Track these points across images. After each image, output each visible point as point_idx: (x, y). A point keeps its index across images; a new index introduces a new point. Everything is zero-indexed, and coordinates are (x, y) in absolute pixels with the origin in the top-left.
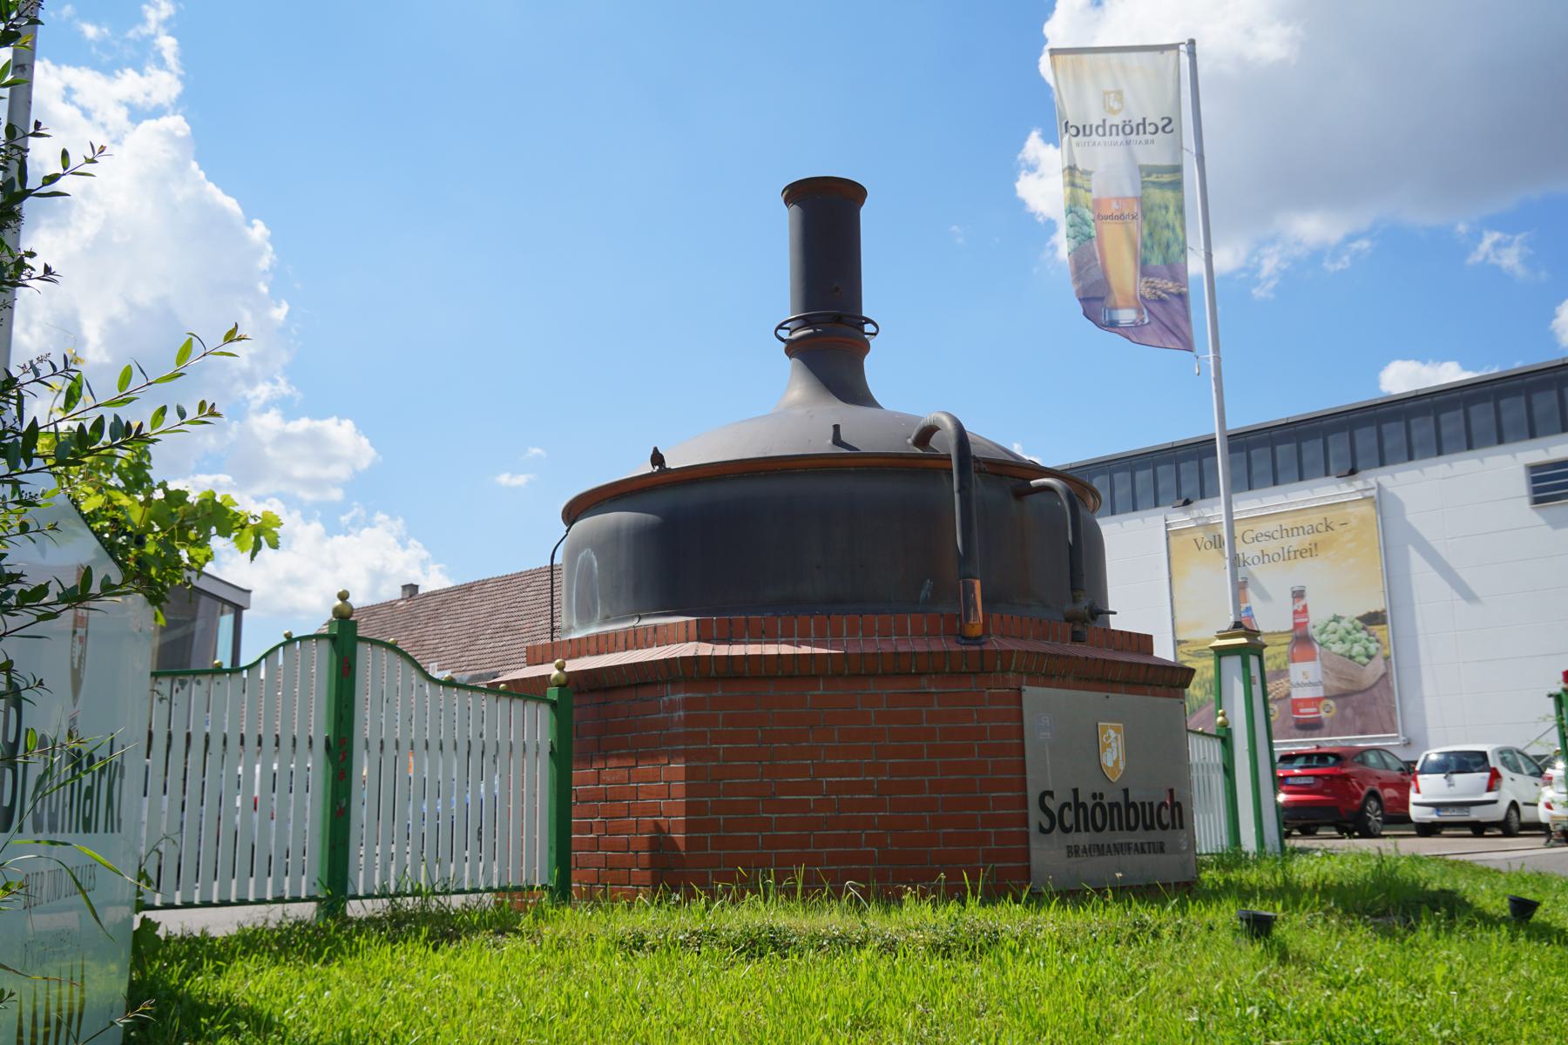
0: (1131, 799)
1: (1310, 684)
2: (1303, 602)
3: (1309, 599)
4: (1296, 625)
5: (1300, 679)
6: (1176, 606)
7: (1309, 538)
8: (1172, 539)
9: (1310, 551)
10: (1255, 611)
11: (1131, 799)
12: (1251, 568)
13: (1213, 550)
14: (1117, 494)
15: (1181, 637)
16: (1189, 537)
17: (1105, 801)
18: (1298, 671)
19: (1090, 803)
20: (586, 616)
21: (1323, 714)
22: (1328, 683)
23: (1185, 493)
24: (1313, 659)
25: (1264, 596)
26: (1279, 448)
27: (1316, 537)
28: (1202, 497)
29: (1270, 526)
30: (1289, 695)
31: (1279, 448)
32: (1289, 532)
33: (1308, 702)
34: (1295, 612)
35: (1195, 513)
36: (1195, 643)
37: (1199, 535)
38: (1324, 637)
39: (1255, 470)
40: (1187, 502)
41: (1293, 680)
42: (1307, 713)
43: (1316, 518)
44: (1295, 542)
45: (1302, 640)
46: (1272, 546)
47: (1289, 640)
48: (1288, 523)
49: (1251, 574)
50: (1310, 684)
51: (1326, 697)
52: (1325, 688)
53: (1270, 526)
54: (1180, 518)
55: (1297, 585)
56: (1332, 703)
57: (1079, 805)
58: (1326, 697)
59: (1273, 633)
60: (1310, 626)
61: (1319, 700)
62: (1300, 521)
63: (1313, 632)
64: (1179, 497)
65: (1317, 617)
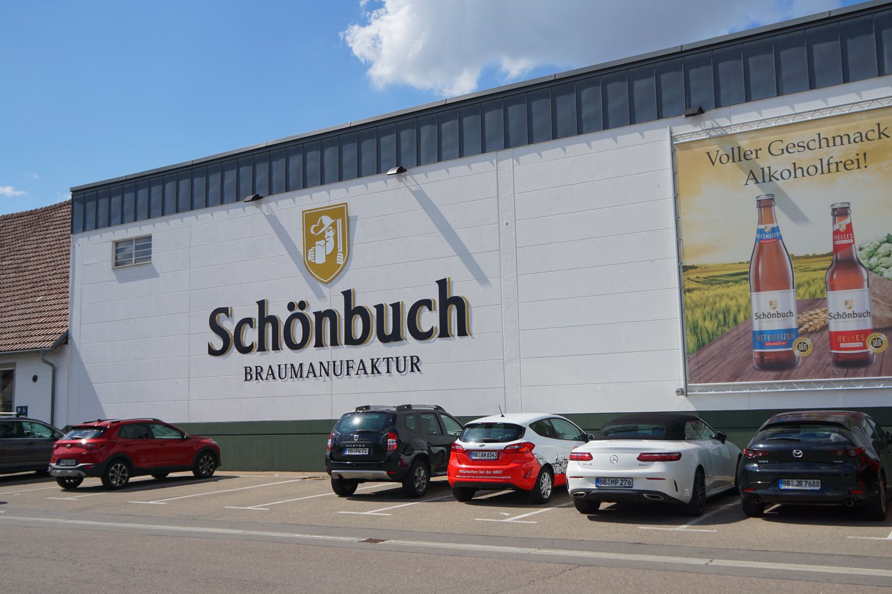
0: (358, 302)
1: (854, 315)
2: (848, 221)
3: (855, 218)
4: (837, 248)
5: (842, 309)
6: (683, 227)
7: (855, 148)
8: (679, 153)
9: (859, 162)
10: (783, 232)
11: (358, 302)
12: (780, 183)
13: (730, 164)
14: (611, 106)
15: (688, 262)
16: (701, 150)
17: (310, 313)
18: (838, 300)
19: (283, 315)
20: (428, 421)
21: (871, 349)
22: (878, 313)
23: (695, 102)
24: (859, 286)
25: (797, 216)
26: (816, 48)
27: (866, 146)
28: (718, 105)
29: (807, 135)
30: (826, 327)
31: (816, 48)
32: (830, 142)
33: (850, 335)
34: (836, 233)
35: (708, 124)
36: (706, 268)
37: (713, 148)
38: (874, 261)
39: (784, 73)
40: (701, 111)
41: (832, 309)
42: (849, 348)
43: (865, 125)
44: (837, 153)
45: (844, 265)
46: (805, 159)
47: (828, 264)
48: (827, 131)
49: (779, 190)
50: (854, 315)
51: (874, 330)
52: (874, 318)
53: (807, 135)
54: (686, 129)
55: (839, 202)
56: (883, 337)
57: (266, 319)
58: (874, 330)
59: (807, 257)
60: (857, 244)
61: (866, 333)
62: (843, 127)
63: (860, 255)
64: (688, 105)
65: (866, 236)
